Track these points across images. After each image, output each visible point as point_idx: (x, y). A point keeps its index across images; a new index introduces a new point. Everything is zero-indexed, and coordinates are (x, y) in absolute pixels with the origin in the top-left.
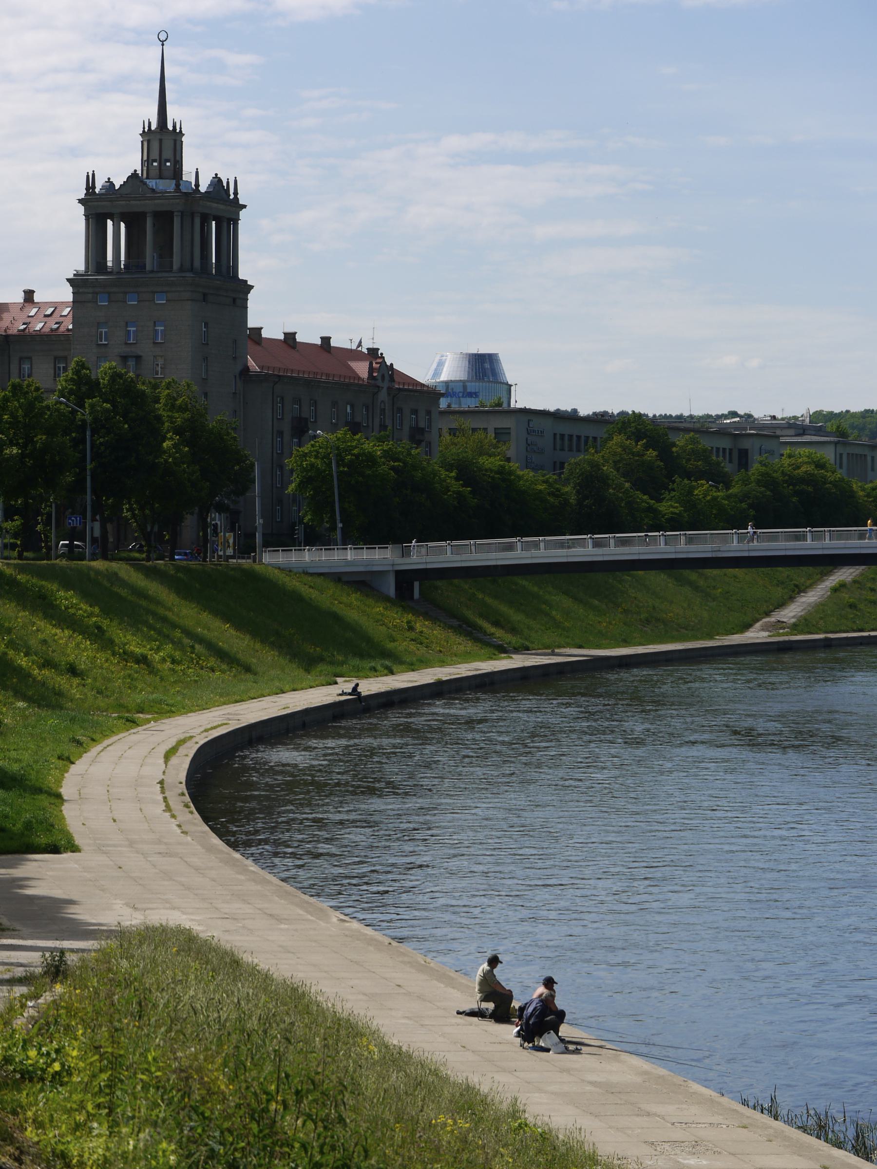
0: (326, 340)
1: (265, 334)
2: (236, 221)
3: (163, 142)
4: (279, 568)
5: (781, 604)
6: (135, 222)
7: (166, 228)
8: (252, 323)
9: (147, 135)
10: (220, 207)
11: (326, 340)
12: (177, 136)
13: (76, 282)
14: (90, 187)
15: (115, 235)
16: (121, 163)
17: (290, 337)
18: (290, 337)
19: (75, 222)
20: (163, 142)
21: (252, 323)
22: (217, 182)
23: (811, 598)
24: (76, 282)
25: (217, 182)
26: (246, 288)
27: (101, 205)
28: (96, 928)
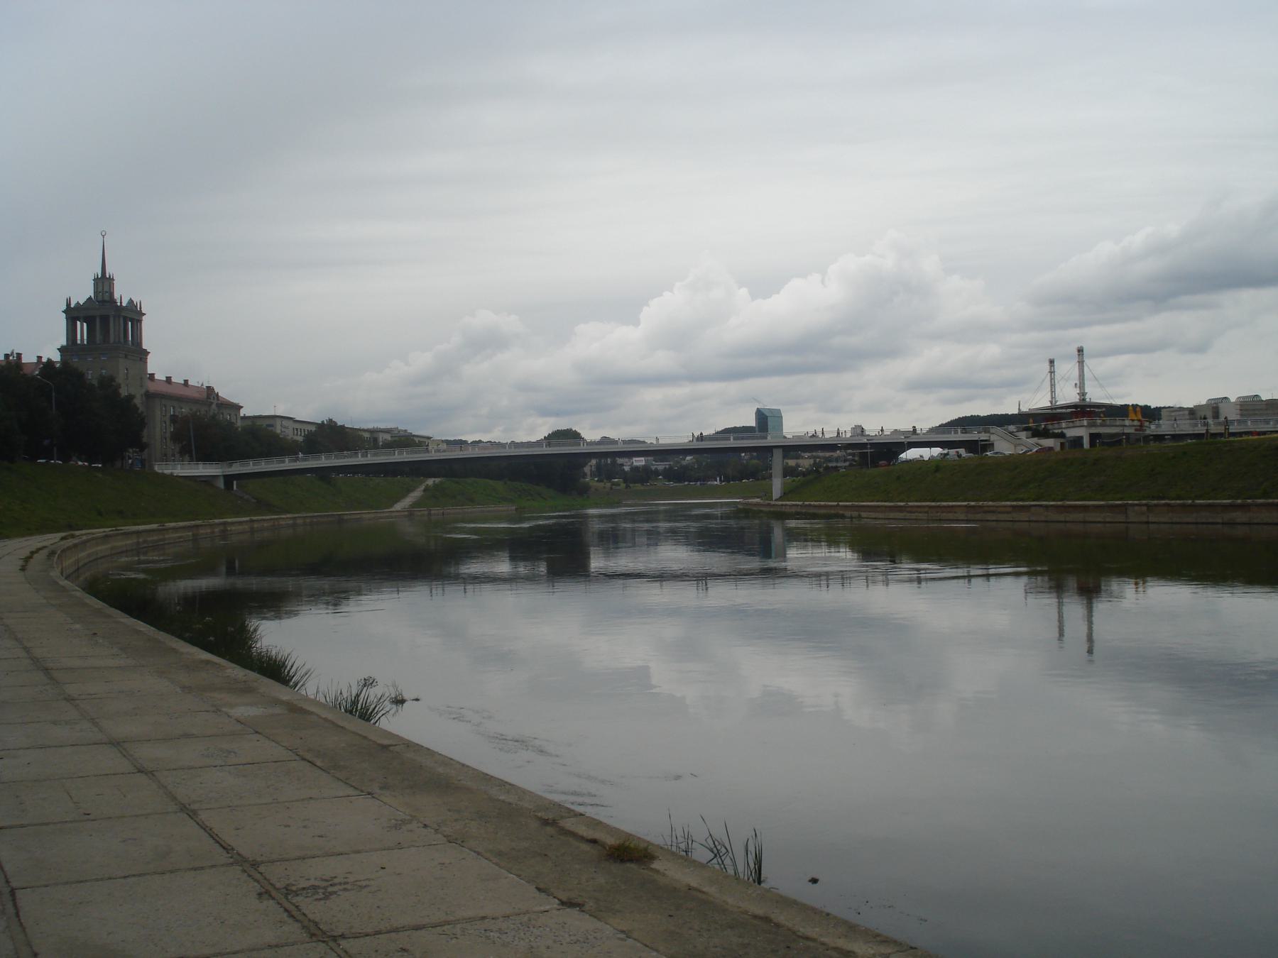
0: (186, 381)
1: (156, 377)
2: (140, 321)
3: (104, 282)
4: (270, 946)
5: (397, 500)
6: (90, 320)
7: (105, 321)
8: (150, 371)
9: (96, 280)
10: (133, 315)
11: (186, 381)
12: (111, 280)
13: (61, 350)
14: (68, 304)
15: (82, 329)
16: (83, 292)
17: (169, 379)
18: (169, 379)
19: (61, 322)
20: (104, 282)
21: (150, 371)
22: (131, 301)
23: (417, 494)
24: (61, 350)
25: (131, 301)
26: (146, 353)
27: (73, 314)
28: (181, 524)
